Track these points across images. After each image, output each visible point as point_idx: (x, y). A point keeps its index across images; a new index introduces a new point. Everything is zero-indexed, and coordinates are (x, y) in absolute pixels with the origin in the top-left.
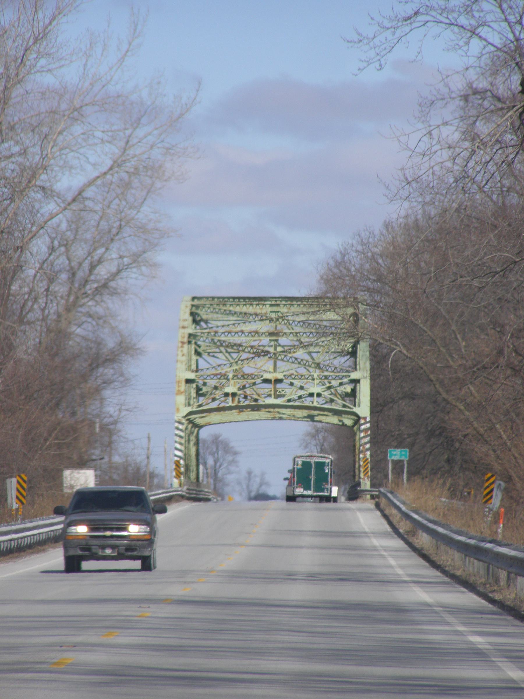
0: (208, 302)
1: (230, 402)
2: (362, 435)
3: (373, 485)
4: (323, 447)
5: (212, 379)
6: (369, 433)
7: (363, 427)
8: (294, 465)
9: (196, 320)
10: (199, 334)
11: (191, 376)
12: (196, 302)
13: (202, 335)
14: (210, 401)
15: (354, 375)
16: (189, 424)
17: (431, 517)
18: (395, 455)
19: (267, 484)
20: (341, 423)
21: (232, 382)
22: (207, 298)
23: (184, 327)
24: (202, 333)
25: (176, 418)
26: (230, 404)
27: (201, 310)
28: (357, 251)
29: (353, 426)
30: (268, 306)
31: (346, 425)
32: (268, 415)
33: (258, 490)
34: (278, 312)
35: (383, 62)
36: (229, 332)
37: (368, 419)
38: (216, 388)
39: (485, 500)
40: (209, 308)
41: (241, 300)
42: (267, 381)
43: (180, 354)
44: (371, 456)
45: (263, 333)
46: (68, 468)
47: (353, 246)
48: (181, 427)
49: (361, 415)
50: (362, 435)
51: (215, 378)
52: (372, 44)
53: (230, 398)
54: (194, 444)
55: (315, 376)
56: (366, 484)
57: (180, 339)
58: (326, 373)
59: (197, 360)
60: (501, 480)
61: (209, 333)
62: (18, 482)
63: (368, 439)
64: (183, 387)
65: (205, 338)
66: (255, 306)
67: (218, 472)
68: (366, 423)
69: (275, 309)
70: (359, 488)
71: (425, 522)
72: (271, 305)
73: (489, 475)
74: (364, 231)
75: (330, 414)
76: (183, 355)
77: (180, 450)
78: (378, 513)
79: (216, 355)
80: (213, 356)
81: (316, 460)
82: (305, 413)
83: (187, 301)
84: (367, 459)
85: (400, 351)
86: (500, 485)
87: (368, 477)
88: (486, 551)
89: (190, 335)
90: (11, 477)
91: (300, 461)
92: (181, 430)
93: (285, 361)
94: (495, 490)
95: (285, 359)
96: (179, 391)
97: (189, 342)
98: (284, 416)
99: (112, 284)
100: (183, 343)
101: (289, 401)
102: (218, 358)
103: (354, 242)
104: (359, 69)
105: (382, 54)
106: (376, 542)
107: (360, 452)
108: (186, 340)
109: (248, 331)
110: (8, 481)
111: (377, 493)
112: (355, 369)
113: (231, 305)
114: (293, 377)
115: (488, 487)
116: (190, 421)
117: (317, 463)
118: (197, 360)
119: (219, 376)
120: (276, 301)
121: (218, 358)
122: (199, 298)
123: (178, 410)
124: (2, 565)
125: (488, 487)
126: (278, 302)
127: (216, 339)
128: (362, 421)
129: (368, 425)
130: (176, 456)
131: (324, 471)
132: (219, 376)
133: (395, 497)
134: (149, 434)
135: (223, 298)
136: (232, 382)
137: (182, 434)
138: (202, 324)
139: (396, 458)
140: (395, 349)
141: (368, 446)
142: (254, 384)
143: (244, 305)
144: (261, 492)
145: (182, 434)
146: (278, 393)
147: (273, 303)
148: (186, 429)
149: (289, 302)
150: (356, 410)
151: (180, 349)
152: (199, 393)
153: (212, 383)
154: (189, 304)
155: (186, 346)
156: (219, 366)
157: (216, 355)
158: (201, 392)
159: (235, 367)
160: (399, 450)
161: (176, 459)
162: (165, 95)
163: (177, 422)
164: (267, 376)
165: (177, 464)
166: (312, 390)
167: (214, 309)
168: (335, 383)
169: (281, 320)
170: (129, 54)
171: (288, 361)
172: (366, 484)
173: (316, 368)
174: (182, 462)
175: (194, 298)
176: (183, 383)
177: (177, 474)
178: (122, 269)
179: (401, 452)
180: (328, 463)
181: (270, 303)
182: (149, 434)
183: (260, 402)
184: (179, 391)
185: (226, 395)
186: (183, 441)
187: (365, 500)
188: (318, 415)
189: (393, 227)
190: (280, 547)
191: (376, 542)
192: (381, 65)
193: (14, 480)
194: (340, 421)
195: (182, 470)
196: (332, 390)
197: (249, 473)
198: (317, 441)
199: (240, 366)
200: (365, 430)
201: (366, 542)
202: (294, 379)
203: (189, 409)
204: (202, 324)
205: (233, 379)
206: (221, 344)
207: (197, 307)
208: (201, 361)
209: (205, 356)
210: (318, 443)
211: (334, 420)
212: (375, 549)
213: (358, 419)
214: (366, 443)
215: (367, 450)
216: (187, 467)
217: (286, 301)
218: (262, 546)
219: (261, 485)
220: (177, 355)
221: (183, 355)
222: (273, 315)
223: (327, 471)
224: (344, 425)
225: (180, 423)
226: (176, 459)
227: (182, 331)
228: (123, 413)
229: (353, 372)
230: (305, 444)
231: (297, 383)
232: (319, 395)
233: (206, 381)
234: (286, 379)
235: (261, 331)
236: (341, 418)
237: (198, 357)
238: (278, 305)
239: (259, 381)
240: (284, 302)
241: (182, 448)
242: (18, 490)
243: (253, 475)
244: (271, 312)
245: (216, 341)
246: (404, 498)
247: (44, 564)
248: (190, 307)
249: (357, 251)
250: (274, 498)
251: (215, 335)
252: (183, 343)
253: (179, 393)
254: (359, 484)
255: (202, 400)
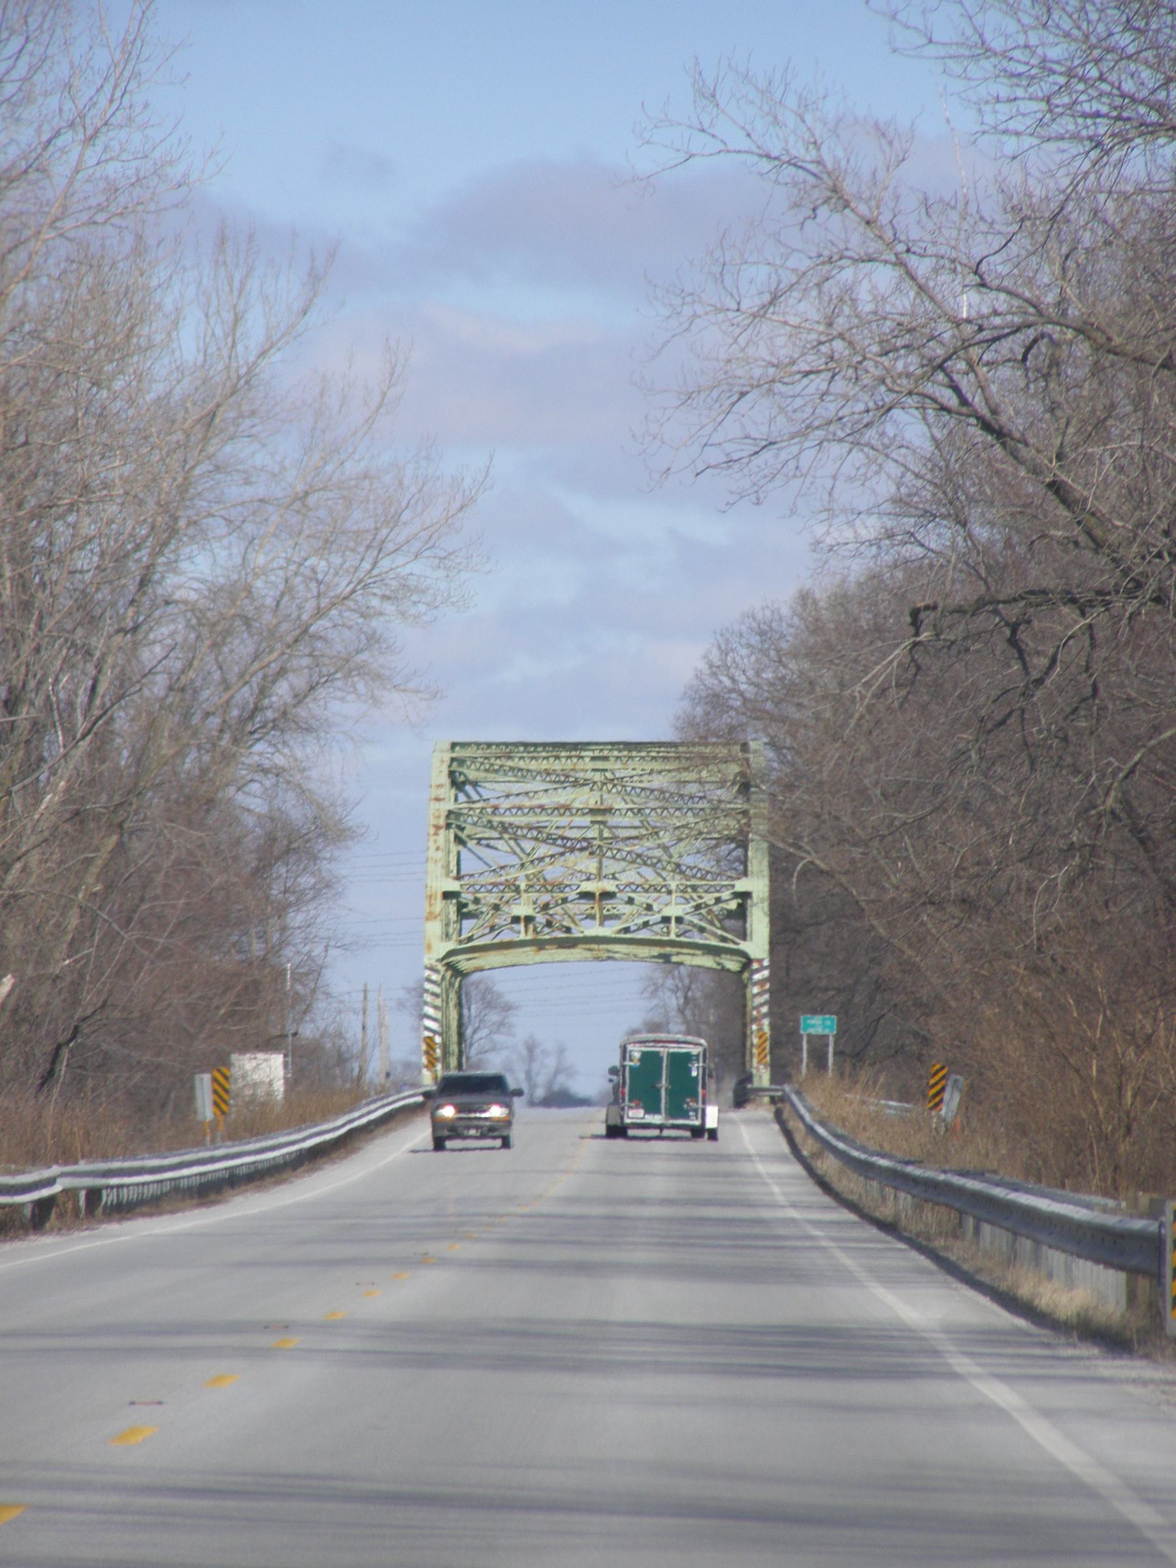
0: (479, 753)
1: (522, 933)
2: (756, 990)
3: (773, 1080)
4: (690, 994)
5: (490, 891)
6: (767, 986)
7: (757, 977)
8: (624, 1058)
9: (457, 783)
10: (465, 811)
11: (454, 886)
12: (459, 753)
13: (471, 813)
14: (487, 930)
15: (741, 885)
16: (446, 970)
17: (840, 1131)
18: (813, 1026)
19: (570, 1072)
20: (719, 967)
21: (524, 896)
22: (478, 744)
23: (437, 799)
24: (470, 809)
25: (426, 962)
26: (522, 937)
27: (469, 767)
28: (749, 646)
29: (741, 972)
30: (587, 760)
31: (728, 970)
32: (588, 954)
33: (550, 1085)
34: (606, 770)
35: (761, 495)
36: (520, 808)
37: (766, 963)
38: (496, 907)
39: (931, 1104)
40: (482, 763)
41: (540, 749)
42: (587, 896)
43: (432, 846)
44: (773, 1026)
45: (578, 810)
46: (244, 1049)
47: (741, 635)
48: (435, 977)
49: (752, 956)
50: (756, 990)
51: (495, 889)
52: (746, 471)
53: (522, 926)
54: (455, 1006)
55: (673, 886)
56: (762, 1077)
57: (433, 821)
58: (694, 882)
59: (459, 854)
60: (957, 1073)
61: (483, 808)
62: (214, 1080)
63: (766, 996)
64: (439, 904)
65: (475, 819)
66: (563, 760)
67: (471, 1045)
68: (762, 968)
69: (600, 765)
70: (749, 1086)
71: (830, 1138)
72: (593, 759)
73: (938, 1067)
74: (763, 609)
75: (699, 952)
76: (438, 849)
77: (435, 1020)
78: (776, 1127)
79: (492, 843)
80: (488, 846)
81: (671, 1050)
82: (656, 951)
83: (442, 751)
84: (765, 1034)
85: (812, 863)
86: (956, 1081)
87: (765, 1065)
88: (960, 1191)
89: (450, 812)
90: (202, 1072)
91: (636, 1052)
92: (434, 982)
93: (618, 860)
94: (949, 1089)
95: (618, 856)
96: (430, 913)
97: (448, 826)
98: (617, 956)
99: (302, 712)
100: (437, 827)
101: (627, 930)
102: (496, 849)
103: (744, 628)
104: (727, 504)
105: (760, 483)
106: (761, 1168)
107: (755, 1020)
108: (442, 822)
109: (553, 806)
110: (197, 1077)
111: (779, 1094)
112: (745, 873)
113: (521, 758)
114: (634, 887)
115: (936, 1084)
116: (449, 966)
117: (673, 1057)
118: (459, 854)
119: (502, 888)
120: (601, 750)
121: (496, 849)
122: (463, 745)
123: (429, 947)
124: (8, 1247)
125: (936, 1084)
126: (606, 753)
127: (496, 819)
128: (755, 966)
129: (766, 973)
130: (427, 1029)
131: (690, 1070)
132: (502, 888)
133: (802, 1100)
134: (365, 985)
135: (507, 745)
136: (524, 896)
137: (437, 990)
138: (468, 788)
139: (812, 1031)
140: (803, 858)
141: (765, 1009)
142: (565, 900)
143: (545, 758)
144: (556, 1088)
145: (437, 990)
146: (605, 912)
147: (597, 753)
148: (443, 978)
149: (625, 753)
150: (744, 946)
151: (432, 838)
152: (463, 913)
153: (492, 899)
154: (447, 756)
155: (442, 832)
156: (502, 868)
157: (492, 843)
158: (465, 910)
159: (531, 871)
160: (821, 1017)
161: (427, 1034)
162: (438, 479)
163: (427, 968)
164: (587, 887)
165: (429, 1042)
166: (667, 912)
167: (492, 765)
168: (709, 899)
169: (610, 786)
170: (382, 410)
171: (624, 859)
172: (761, 1077)
173: (673, 871)
174: (438, 1039)
175: (454, 745)
176: (439, 896)
177: (430, 1062)
178: (317, 684)
179: (824, 1020)
180: (698, 1056)
181: (590, 754)
182: (365, 985)
183: (576, 934)
184: (430, 913)
185: (516, 920)
186: (438, 1002)
187: (760, 1105)
188: (678, 954)
189: (815, 602)
190: (620, 1174)
191: (761, 1168)
192: (758, 499)
193: (207, 1077)
194: (718, 964)
195: (439, 1052)
196: (703, 911)
197: (531, 1048)
198: (677, 981)
199: (538, 869)
200: (761, 983)
201: (747, 1167)
202: (634, 891)
203: (451, 945)
204: (468, 788)
205: (526, 891)
206: (504, 828)
207: (461, 762)
208: (464, 853)
209: (471, 844)
210: (680, 985)
211: (708, 962)
212: (757, 1175)
213: (747, 962)
214: (762, 1005)
215: (765, 1016)
216: (445, 1047)
217: (620, 751)
218: (592, 1172)
219: (557, 1072)
220: (428, 849)
221: (438, 849)
222: (598, 777)
223: (694, 1074)
224: (724, 970)
225: (432, 969)
226: (427, 1034)
227: (434, 805)
228: (333, 952)
229: (738, 879)
230: (651, 989)
231: (640, 898)
232: (679, 920)
233: (479, 895)
234: (621, 891)
235: (577, 805)
236: (717, 959)
237: (460, 848)
238: (606, 758)
239: (572, 895)
240: (616, 753)
241: (438, 1015)
242: (215, 1092)
243: (537, 1051)
244: (594, 770)
245: (495, 824)
246: (811, 1102)
247: (18, 1262)
248: (447, 763)
249: (749, 646)
250: (584, 1102)
251: (493, 813)
252: (437, 827)
253: (431, 916)
254: (749, 1078)
255: (468, 924)
